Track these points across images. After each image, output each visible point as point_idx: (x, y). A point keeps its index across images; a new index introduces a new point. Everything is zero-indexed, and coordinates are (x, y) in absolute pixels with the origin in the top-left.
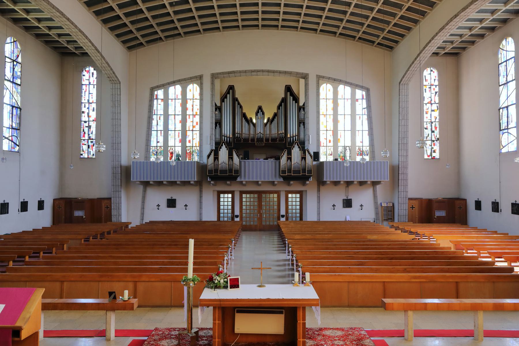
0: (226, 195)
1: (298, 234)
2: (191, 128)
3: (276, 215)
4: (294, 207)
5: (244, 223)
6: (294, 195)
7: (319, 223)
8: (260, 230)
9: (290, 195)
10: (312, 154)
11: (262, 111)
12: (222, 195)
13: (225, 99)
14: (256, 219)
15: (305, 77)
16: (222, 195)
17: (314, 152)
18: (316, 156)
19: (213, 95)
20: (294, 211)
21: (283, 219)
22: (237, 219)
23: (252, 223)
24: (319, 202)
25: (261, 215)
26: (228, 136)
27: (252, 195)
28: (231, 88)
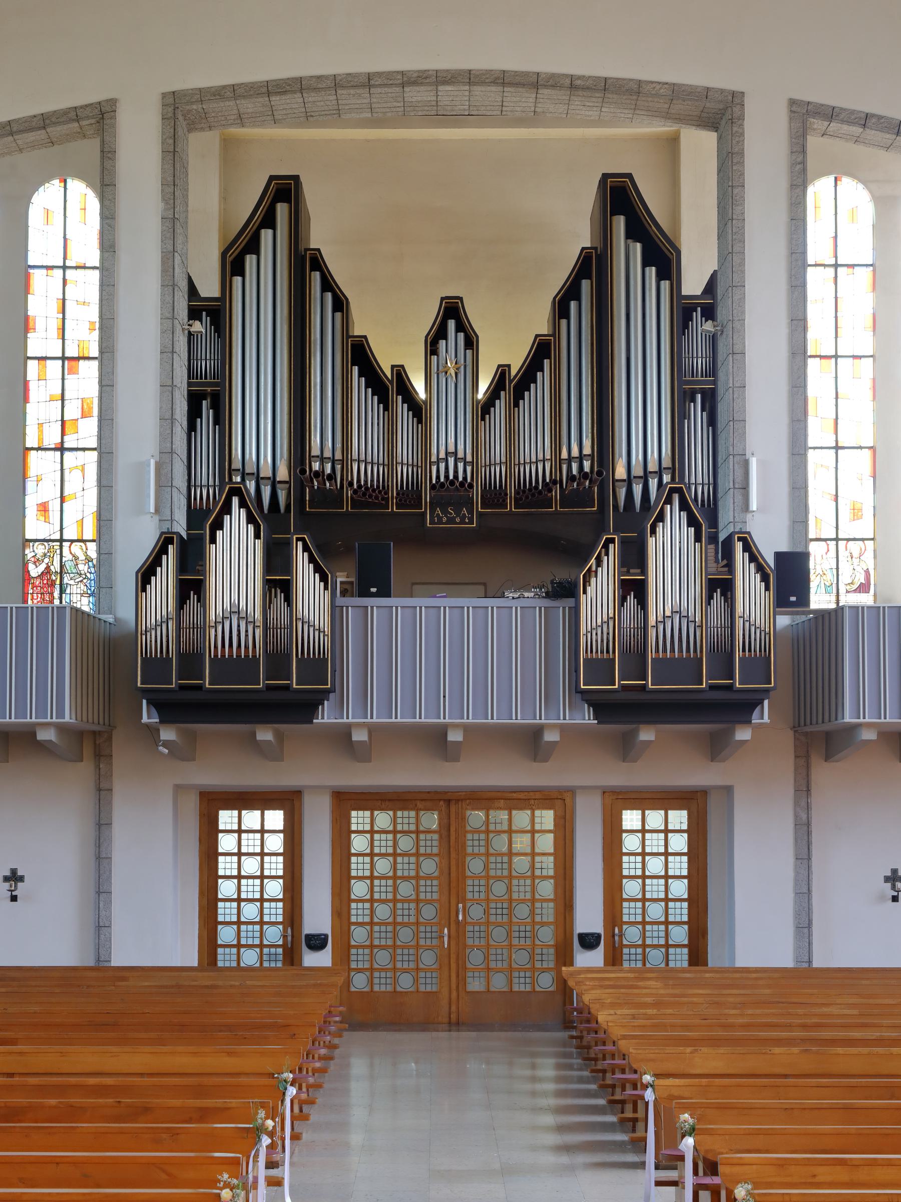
0: (252, 819)
1: (715, 1042)
2: (52, 437)
3: (547, 935)
4: (655, 889)
5: (359, 982)
6: (655, 818)
7: (804, 978)
8: (455, 1024)
9: (631, 819)
10: (771, 561)
11: (461, 327)
12: (227, 818)
13: (250, 260)
14: (428, 959)
15: (720, 114)
16: (227, 818)
17: (778, 556)
18: (789, 577)
19: (174, 223)
20: (655, 911)
21: (593, 959)
22: (321, 959)
23: (406, 982)
24: (804, 856)
25: (459, 931)
26: (266, 472)
27: (406, 818)
28: (284, 191)
